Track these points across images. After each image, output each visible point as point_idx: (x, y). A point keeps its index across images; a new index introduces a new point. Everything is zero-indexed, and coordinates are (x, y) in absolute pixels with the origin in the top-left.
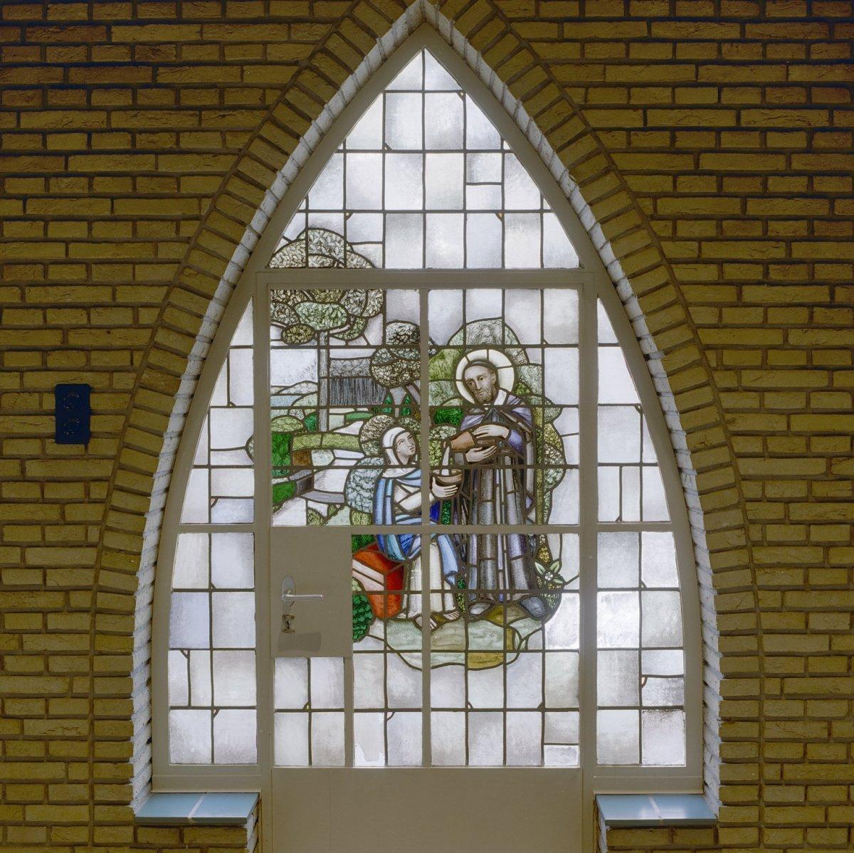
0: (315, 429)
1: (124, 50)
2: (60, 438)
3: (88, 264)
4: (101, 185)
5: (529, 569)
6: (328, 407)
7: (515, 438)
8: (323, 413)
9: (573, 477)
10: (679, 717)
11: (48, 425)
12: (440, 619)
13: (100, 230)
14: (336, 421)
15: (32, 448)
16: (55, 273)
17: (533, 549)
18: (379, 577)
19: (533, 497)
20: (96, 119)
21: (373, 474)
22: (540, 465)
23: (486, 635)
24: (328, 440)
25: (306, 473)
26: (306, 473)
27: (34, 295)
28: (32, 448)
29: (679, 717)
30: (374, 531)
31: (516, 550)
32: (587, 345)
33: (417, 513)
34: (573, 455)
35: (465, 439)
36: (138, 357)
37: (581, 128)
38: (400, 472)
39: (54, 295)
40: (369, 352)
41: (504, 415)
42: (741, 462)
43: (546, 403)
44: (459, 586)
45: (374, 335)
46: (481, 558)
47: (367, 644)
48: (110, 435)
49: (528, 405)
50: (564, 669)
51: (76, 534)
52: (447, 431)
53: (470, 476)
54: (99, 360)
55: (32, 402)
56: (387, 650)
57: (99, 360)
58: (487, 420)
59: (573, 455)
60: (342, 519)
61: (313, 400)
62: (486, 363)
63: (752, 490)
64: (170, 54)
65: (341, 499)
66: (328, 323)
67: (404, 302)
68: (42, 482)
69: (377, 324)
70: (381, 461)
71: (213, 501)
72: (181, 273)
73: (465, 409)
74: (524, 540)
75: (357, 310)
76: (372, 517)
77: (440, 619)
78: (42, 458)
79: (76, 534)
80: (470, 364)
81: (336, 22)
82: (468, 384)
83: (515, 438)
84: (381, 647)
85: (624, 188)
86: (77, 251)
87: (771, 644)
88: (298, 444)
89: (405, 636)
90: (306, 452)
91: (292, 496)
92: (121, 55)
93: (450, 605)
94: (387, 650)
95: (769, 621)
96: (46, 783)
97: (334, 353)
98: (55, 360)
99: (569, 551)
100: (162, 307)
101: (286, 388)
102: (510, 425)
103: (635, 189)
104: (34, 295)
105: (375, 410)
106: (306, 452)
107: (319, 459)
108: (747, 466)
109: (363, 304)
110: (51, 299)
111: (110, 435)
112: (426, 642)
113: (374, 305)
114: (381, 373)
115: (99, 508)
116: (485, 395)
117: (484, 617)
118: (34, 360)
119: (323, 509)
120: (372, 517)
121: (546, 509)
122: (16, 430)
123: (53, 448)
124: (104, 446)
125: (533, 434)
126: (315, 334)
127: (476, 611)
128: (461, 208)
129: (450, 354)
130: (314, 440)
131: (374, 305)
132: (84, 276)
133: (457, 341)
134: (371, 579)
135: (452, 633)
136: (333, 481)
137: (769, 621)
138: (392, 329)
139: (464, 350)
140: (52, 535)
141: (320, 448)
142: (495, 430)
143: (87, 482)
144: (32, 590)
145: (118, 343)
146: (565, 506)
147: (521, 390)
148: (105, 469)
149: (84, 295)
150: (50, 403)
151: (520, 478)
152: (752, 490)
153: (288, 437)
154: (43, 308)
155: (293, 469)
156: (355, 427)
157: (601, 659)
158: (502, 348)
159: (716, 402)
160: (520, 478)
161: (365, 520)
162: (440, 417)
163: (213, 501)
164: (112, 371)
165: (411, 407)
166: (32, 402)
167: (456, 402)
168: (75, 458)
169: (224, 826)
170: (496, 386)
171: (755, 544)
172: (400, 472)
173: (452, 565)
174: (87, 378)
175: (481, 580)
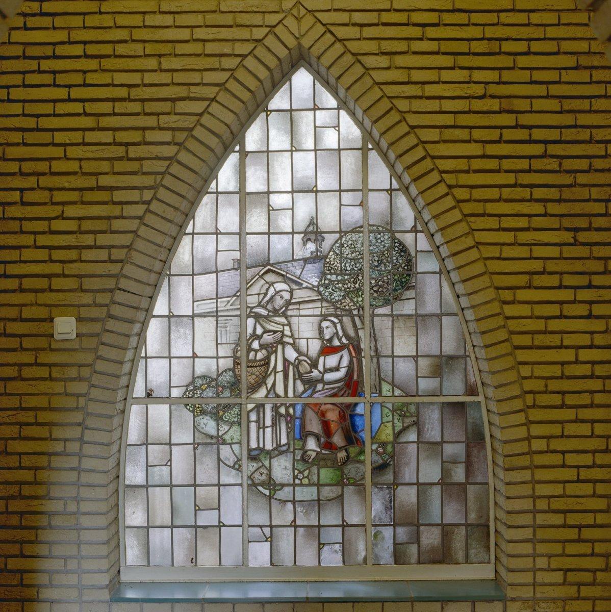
37: (415, 141)
42: (518, 352)
55: (221, 322)
63: (525, 371)
71: (169, 464)
80: (337, 369)
81: (244, 56)
85: (347, 51)
87: (540, 475)
95: (539, 460)
101: (363, 309)
103: (441, 168)
108: (522, 356)
128: (220, 196)
137: (539, 460)
152: (525, 371)
163: (169, 464)
166: (221, 322)
169: (277, 602)
171: (529, 407)
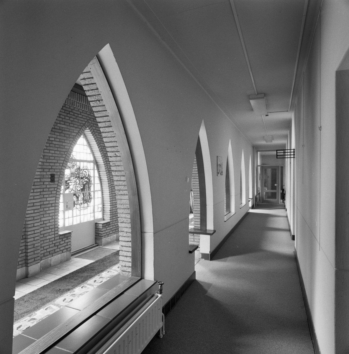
0: (69, 180)
1: (59, 127)
2: (51, 182)
3: (55, 157)
4: (56, 146)
5: (89, 196)
6: (71, 177)
7: (88, 181)
8: (71, 178)
9: (93, 185)
10: (101, 212)
11: (49, 180)
12: (81, 204)
13: (56, 152)
14: (72, 179)
15: (48, 183)
16: (51, 158)
17: (89, 194)
18: (76, 199)
19: (89, 188)
20: (56, 136)
21: (75, 186)
22: (90, 184)
23: (86, 205)
24: (71, 181)
25: (69, 186)
26: (69, 186)
27: (48, 161)
28: (48, 183)
29: (101, 212)
30: (75, 193)
31: (88, 195)
32: (94, 169)
33: (79, 190)
34: (93, 183)
35: (84, 181)
36: (60, 170)
38: (78, 185)
39: (50, 161)
40: (75, 170)
41: (87, 178)
43: (91, 177)
44: (83, 199)
45: (75, 168)
46: (85, 196)
47: (75, 208)
48: (57, 181)
49: (89, 177)
50: (92, 208)
51: (53, 195)
52: (82, 180)
53: (84, 185)
54: (56, 170)
55: (48, 176)
56: (77, 208)
57: (56, 170)
58: (86, 179)
59: (93, 183)
60: (72, 192)
61: (69, 176)
62: (85, 172)
64: (64, 129)
65: (72, 189)
66: (71, 166)
67: (78, 163)
68: (49, 188)
69: (75, 166)
70: (76, 184)
72: (65, 159)
73: (84, 177)
74: (89, 193)
75: (73, 164)
76: (75, 191)
77: (81, 204)
78: (49, 185)
79: (53, 195)
82: (84, 174)
83: (88, 181)
84: (76, 208)
86: (53, 155)
88: (68, 182)
89: (78, 206)
90: (69, 183)
91: (67, 189)
92: (58, 128)
93: (82, 202)
94: (77, 208)
96: (49, 233)
97: (71, 170)
98: (51, 170)
99: (92, 194)
100: (63, 163)
102: (88, 179)
104: (48, 161)
105: (76, 177)
106: (69, 183)
107: (70, 184)
109: (74, 164)
110: (50, 162)
111: (57, 181)
112: (80, 207)
113: (75, 164)
114: (76, 173)
115: (56, 191)
116: (85, 175)
117: (86, 203)
118: (48, 170)
119: (70, 191)
120: (75, 191)
121: (90, 189)
122: (46, 181)
123: (50, 183)
124: (56, 183)
125: (89, 180)
126: (69, 167)
127: (85, 202)
129: (82, 170)
130: (69, 182)
131: (75, 164)
132: (54, 158)
133: (83, 169)
134: (75, 198)
135: (82, 205)
136: (71, 187)
138: (77, 167)
139: (83, 170)
140: (50, 196)
141: (70, 182)
142: (86, 180)
143: (54, 188)
144: (47, 204)
145: (58, 168)
146: (92, 189)
147: (89, 175)
148: (56, 186)
149: (54, 161)
150: (50, 176)
151: (88, 185)
153: (67, 181)
154: (49, 163)
155: (67, 185)
156: (74, 180)
157: (95, 206)
158: (87, 170)
159: (109, 176)
160: (88, 185)
161: (74, 192)
162: (82, 178)
164: (57, 172)
165: (79, 177)
166: (48, 176)
167: (83, 176)
168: (53, 184)
170: (86, 174)
172: (78, 185)
173: (83, 197)
174: (54, 173)
175: (85, 198)
